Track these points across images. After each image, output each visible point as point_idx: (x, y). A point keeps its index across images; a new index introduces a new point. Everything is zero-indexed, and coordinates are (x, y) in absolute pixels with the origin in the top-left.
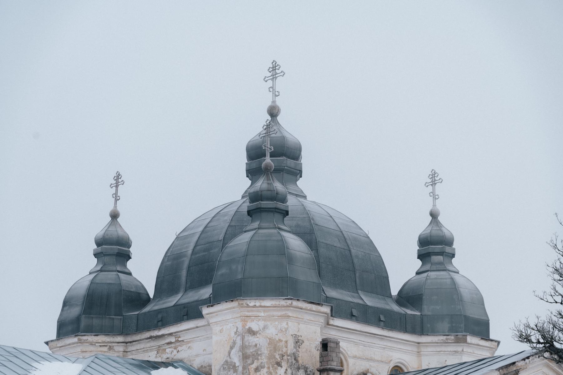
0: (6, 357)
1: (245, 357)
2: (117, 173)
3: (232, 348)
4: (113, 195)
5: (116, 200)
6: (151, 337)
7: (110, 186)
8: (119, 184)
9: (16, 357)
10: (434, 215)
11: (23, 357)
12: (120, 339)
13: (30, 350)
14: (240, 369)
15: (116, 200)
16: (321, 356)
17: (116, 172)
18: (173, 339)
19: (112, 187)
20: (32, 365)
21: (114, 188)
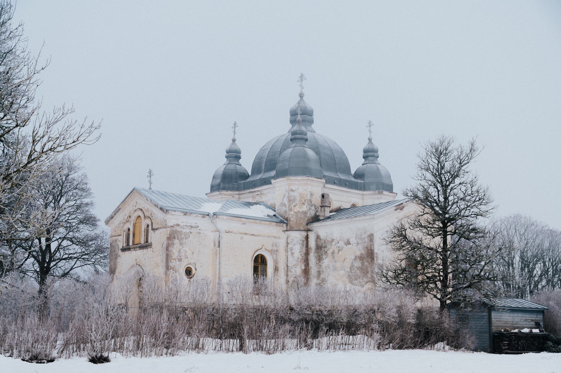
1: (290, 201)
3: (284, 197)
6: (250, 192)
10: (370, 140)
12: (237, 192)
14: (288, 206)
16: (322, 200)
18: (259, 193)
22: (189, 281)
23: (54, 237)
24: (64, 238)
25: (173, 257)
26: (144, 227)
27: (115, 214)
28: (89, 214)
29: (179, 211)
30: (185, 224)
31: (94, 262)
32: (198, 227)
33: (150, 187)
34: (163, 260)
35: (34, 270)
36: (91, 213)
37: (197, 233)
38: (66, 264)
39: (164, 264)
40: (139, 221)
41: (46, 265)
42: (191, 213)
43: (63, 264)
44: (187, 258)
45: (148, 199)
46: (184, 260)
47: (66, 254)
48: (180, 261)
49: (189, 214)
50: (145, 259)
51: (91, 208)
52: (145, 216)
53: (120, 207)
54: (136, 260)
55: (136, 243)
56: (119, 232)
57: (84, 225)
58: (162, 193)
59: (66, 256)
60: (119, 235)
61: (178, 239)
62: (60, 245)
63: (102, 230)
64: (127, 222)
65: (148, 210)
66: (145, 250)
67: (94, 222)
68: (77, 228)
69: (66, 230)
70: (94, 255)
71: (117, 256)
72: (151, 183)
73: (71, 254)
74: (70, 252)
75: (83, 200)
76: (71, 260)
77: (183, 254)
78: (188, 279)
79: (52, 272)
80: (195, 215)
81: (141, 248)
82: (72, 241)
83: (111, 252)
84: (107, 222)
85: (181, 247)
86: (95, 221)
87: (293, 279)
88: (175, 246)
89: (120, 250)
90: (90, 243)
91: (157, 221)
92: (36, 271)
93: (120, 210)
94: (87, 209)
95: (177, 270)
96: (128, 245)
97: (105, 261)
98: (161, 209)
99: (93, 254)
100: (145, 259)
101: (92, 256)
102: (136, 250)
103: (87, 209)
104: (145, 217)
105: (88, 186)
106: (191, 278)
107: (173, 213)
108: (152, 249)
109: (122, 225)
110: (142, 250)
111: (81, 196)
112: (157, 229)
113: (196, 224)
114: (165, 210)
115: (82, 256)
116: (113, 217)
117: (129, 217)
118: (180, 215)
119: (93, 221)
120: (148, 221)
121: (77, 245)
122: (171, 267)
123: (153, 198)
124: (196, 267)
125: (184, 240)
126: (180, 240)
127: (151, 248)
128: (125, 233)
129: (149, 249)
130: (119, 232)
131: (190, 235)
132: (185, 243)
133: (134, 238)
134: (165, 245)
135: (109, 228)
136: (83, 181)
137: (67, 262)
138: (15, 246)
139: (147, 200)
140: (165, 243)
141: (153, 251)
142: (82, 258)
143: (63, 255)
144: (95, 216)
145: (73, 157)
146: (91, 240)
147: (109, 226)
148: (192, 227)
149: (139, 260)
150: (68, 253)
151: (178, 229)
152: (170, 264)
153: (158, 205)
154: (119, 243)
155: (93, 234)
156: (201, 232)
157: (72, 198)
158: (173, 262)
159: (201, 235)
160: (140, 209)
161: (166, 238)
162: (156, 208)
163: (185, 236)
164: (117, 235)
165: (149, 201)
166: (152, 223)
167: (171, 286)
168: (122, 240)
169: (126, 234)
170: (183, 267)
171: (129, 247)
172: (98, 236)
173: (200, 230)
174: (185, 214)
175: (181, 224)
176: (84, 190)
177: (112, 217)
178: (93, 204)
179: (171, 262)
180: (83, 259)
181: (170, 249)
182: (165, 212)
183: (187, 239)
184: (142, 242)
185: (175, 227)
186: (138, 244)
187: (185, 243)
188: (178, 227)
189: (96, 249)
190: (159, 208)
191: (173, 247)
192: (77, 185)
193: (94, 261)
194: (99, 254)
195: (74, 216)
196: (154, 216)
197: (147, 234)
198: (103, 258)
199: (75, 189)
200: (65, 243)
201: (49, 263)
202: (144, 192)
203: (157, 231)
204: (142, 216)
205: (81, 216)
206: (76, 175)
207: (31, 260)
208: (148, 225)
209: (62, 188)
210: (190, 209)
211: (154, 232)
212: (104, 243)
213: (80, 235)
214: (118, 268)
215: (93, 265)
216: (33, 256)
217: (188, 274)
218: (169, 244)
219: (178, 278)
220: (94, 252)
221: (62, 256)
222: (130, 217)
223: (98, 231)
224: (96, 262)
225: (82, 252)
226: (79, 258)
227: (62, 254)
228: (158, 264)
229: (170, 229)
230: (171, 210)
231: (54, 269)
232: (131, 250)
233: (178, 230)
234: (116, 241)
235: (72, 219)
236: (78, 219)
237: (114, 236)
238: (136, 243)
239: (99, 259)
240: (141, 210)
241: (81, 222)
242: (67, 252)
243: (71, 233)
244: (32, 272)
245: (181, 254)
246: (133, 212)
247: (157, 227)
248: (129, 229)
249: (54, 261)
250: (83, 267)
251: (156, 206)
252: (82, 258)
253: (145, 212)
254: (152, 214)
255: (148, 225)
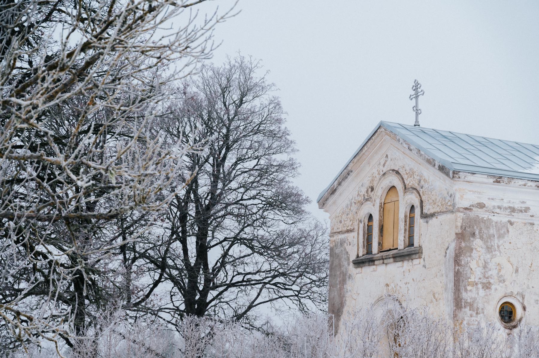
0: (510, 151)
2: (415, 82)
4: (413, 108)
5: (417, 114)
7: (410, 97)
8: (419, 94)
9: (519, 151)
11: (525, 151)
13: (531, 145)
15: (417, 114)
17: (414, 81)
19: (412, 99)
20: (534, 158)
21: (414, 100)
22: (509, 334)
23: (213, 237)
24: (236, 240)
25: (472, 279)
26: (403, 211)
27: (340, 184)
28: (286, 187)
29: (482, 173)
30: (496, 203)
31: (299, 292)
32: (527, 209)
33: (417, 121)
34: (446, 285)
35: (172, 307)
36: (291, 185)
37: (525, 224)
38: (240, 295)
39: (450, 295)
40: (392, 197)
41: (197, 297)
42: (511, 178)
43: (233, 297)
44: (504, 281)
45: (411, 148)
46: (498, 287)
47: (239, 274)
48: (488, 288)
49: (506, 180)
50: (406, 284)
51: (291, 175)
52: (405, 186)
53: (349, 168)
54: (387, 285)
55: (386, 246)
56: (348, 223)
57: (277, 211)
58: (444, 134)
59: (239, 278)
60: (348, 231)
61: (481, 238)
62: (225, 255)
63: (313, 222)
64: (367, 200)
65: (412, 173)
66: (406, 263)
67: (295, 204)
68: (262, 217)
69: (239, 222)
70: (298, 277)
71: (345, 278)
72: (417, 111)
73: (249, 273)
74: (248, 270)
75: (274, 156)
76: (249, 287)
77: (493, 272)
78: (507, 331)
79: (212, 313)
80: (521, 182)
81: (398, 259)
82: (252, 248)
83: (331, 269)
84: (323, 202)
85: (489, 256)
86: (298, 202)
87: (24, 206)
88: (475, 254)
89: (351, 264)
90: (290, 250)
91: (433, 198)
92: (177, 309)
93: (351, 174)
94: (281, 176)
95: (480, 310)
96: (369, 251)
97: (321, 289)
98: (442, 169)
99: (296, 274)
100: (406, 284)
101: (294, 279)
102: (386, 264)
103: (281, 176)
104: (405, 188)
105: (283, 127)
106: (515, 327)
107: (470, 178)
108: (422, 260)
109: (354, 208)
110: (399, 264)
111: (270, 148)
112: (432, 215)
113: (523, 202)
114: (451, 173)
115: (274, 277)
116: (335, 190)
117: (370, 190)
118: (486, 183)
119: (293, 202)
120: (413, 199)
121: (261, 254)
122: (466, 302)
123: (424, 145)
124: (526, 304)
125: (496, 241)
126: (487, 239)
127: (420, 258)
128: (361, 225)
129: (416, 261)
130: (349, 224)
131: (510, 228)
132: (498, 247)
133: (382, 236)
134: (451, 252)
135: (328, 215)
136: (273, 115)
137: (242, 291)
138: (132, 255)
139: (411, 150)
140: (453, 246)
141: (424, 266)
142: (271, 283)
143: (233, 277)
144: (299, 193)
145: (251, 63)
146: (291, 245)
147: (326, 211)
148: (513, 210)
149: (392, 285)
150: (243, 272)
151: (482, 214)
152: (465, 295)
153: (434, 160)
154: (348, 248)
155: (294, 230)
156: (535, 223)
157: (250, 152)
158: (471, 290)
159: (535, 229)
160: (393, 170)
161: (453, 236)
162: (430, 167)
163: (498, 230)
164: (345, 229)
165: (415, 152)
166: (422, 202)
167: (466, 345)
168: (356, 240)
169: (364, 227)
170: (495, 302)
171: (370, 256)
172: (305, 235)
173: (532, 216)
174: (498, 179)
175: (490, 204)
176: (275, 134)
177: (333, 191)
178: (295, 167)
179: (466, 290)
180: (275, 284)
181: (464, 260)
182: (451, 176)
183: (503, 237)
184: (401, 245)
185: (474, 209)
186: (390, 250)
187: (498, 247)
188: (480, 210)
189: (301, 264)
190: (437, 166)
191: (470, 256)
192: (261, 123)
193: (298, 289)
194: (309, 275)
195: (253, 192)
196: (426, 186)
197: (410, 227)
198: (317, 283)
199: (256, 133)
200: (237, 250)
201: (204, 293)
202: (404, 132)
203: (434, 219)
204: (400, 187)
205: (269, 193)
206: (257, 103)
207: (166, 286)
208: (413, 207)
209: (228, 130)
210: (508, 169)
211: (427, 222)
212: (318, 251)
213: (267, 234)
214: (348, 303)
215: (296, 298)
216: (172, 278)
217: (507, 318)
218: (460, 248)
219: (483, 325)
220: (297, 271)
221: (229, 279)
222: (372, 189)
223: (305, 225)
224: (301, 292)
225: (271, 270)
226: (265, 283)
227: (230, 274)
228: (436, 296)
229: (462, 214)
230: (465, 171)
231: (215, 306)
232: (376, 262)
233: (481, 216)
234: (342, 242)
235: (249, 199)
236: (261, 198)
237: (339, 233)
238: (386, 246)
239: (309, 286)
240: (397, 172)
241: (271, 204)
242: (241, 270)
243: (247, 230)
244: (168, 311)
245: (490, 273)
246: (378, 177)
247: (432, 211)
248: (371, 217)
249: (215, 287)
250: (274, 302)
251: (431, 162)
252: (271, 283)
253: (405, 177)
254: (422, 183)
255: (413, 207)
